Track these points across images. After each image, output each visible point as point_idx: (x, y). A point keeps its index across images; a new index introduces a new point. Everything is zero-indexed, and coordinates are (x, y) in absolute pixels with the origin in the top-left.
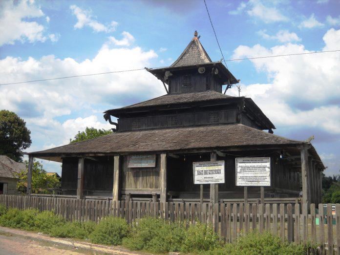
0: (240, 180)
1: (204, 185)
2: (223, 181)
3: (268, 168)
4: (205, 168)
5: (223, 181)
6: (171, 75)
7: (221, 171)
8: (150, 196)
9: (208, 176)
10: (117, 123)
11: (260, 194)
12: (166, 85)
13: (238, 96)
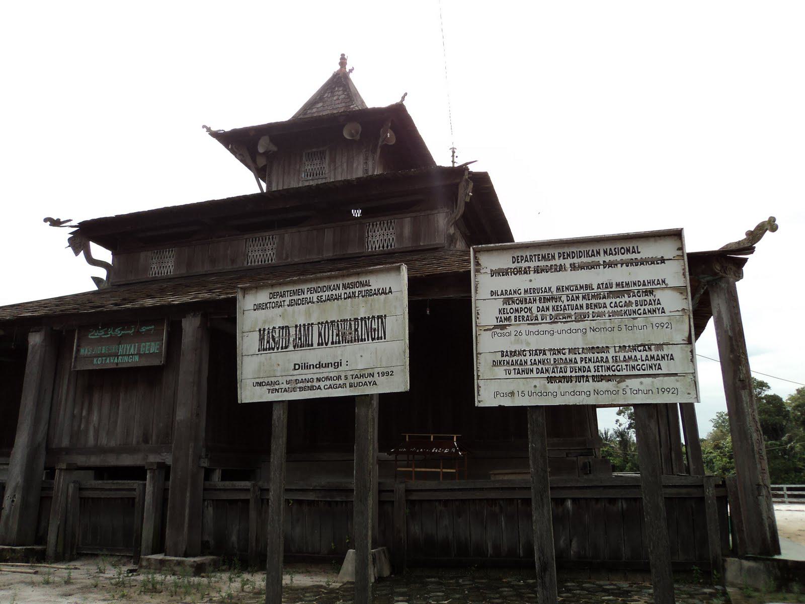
0: (500, 372)
1: (292, 405)
2: (400, 383)
3: (680, 290)
4: (299, 315)
5: (400, 383)
6: (274, 148)
7: (389, 322)
8: (138, 473)
9: (312, 356)
10: (110, 262)
11: (171, 447)
12: (261, 182)
13: (450, 165)
